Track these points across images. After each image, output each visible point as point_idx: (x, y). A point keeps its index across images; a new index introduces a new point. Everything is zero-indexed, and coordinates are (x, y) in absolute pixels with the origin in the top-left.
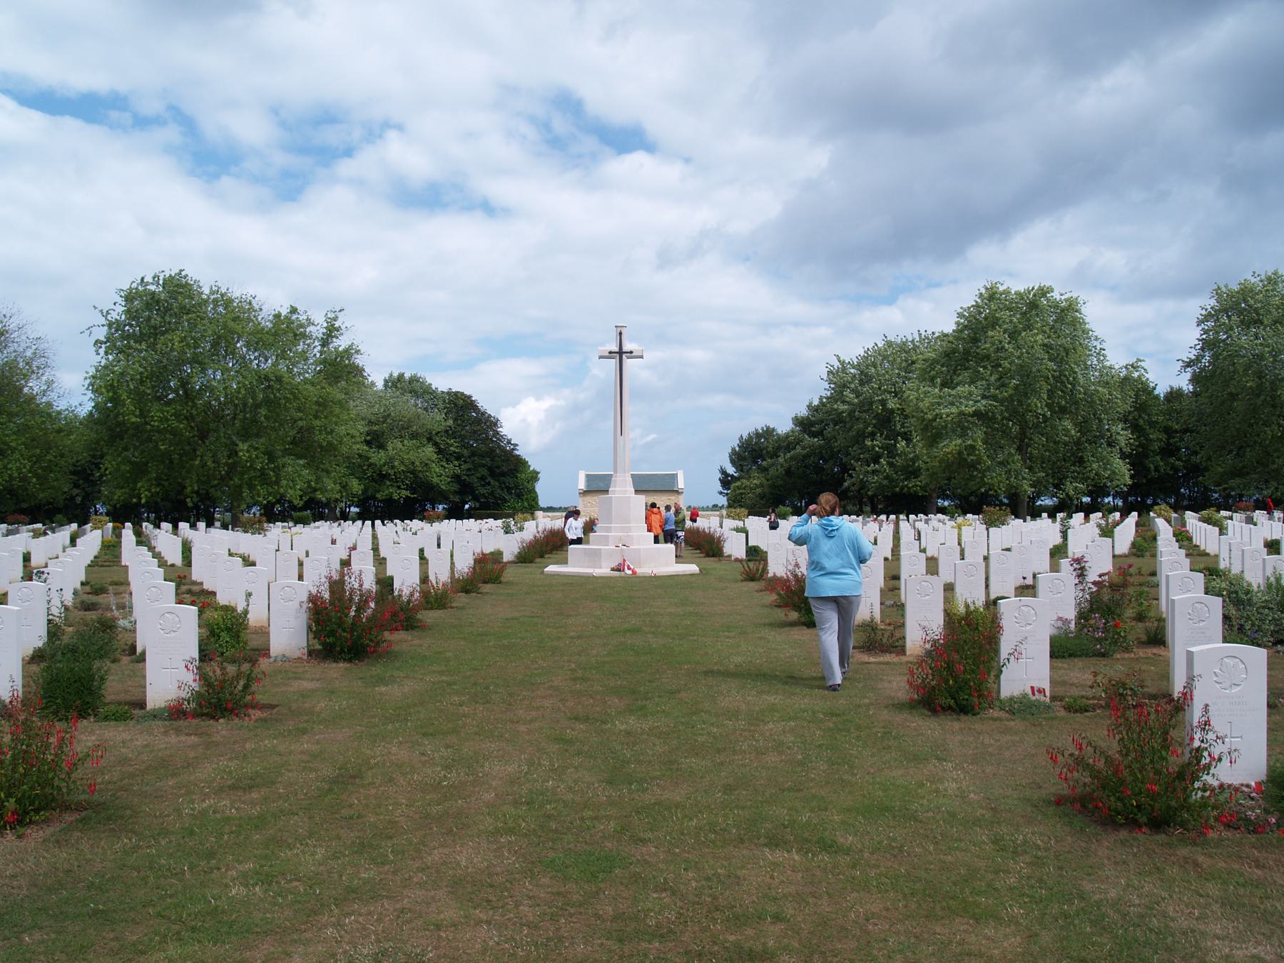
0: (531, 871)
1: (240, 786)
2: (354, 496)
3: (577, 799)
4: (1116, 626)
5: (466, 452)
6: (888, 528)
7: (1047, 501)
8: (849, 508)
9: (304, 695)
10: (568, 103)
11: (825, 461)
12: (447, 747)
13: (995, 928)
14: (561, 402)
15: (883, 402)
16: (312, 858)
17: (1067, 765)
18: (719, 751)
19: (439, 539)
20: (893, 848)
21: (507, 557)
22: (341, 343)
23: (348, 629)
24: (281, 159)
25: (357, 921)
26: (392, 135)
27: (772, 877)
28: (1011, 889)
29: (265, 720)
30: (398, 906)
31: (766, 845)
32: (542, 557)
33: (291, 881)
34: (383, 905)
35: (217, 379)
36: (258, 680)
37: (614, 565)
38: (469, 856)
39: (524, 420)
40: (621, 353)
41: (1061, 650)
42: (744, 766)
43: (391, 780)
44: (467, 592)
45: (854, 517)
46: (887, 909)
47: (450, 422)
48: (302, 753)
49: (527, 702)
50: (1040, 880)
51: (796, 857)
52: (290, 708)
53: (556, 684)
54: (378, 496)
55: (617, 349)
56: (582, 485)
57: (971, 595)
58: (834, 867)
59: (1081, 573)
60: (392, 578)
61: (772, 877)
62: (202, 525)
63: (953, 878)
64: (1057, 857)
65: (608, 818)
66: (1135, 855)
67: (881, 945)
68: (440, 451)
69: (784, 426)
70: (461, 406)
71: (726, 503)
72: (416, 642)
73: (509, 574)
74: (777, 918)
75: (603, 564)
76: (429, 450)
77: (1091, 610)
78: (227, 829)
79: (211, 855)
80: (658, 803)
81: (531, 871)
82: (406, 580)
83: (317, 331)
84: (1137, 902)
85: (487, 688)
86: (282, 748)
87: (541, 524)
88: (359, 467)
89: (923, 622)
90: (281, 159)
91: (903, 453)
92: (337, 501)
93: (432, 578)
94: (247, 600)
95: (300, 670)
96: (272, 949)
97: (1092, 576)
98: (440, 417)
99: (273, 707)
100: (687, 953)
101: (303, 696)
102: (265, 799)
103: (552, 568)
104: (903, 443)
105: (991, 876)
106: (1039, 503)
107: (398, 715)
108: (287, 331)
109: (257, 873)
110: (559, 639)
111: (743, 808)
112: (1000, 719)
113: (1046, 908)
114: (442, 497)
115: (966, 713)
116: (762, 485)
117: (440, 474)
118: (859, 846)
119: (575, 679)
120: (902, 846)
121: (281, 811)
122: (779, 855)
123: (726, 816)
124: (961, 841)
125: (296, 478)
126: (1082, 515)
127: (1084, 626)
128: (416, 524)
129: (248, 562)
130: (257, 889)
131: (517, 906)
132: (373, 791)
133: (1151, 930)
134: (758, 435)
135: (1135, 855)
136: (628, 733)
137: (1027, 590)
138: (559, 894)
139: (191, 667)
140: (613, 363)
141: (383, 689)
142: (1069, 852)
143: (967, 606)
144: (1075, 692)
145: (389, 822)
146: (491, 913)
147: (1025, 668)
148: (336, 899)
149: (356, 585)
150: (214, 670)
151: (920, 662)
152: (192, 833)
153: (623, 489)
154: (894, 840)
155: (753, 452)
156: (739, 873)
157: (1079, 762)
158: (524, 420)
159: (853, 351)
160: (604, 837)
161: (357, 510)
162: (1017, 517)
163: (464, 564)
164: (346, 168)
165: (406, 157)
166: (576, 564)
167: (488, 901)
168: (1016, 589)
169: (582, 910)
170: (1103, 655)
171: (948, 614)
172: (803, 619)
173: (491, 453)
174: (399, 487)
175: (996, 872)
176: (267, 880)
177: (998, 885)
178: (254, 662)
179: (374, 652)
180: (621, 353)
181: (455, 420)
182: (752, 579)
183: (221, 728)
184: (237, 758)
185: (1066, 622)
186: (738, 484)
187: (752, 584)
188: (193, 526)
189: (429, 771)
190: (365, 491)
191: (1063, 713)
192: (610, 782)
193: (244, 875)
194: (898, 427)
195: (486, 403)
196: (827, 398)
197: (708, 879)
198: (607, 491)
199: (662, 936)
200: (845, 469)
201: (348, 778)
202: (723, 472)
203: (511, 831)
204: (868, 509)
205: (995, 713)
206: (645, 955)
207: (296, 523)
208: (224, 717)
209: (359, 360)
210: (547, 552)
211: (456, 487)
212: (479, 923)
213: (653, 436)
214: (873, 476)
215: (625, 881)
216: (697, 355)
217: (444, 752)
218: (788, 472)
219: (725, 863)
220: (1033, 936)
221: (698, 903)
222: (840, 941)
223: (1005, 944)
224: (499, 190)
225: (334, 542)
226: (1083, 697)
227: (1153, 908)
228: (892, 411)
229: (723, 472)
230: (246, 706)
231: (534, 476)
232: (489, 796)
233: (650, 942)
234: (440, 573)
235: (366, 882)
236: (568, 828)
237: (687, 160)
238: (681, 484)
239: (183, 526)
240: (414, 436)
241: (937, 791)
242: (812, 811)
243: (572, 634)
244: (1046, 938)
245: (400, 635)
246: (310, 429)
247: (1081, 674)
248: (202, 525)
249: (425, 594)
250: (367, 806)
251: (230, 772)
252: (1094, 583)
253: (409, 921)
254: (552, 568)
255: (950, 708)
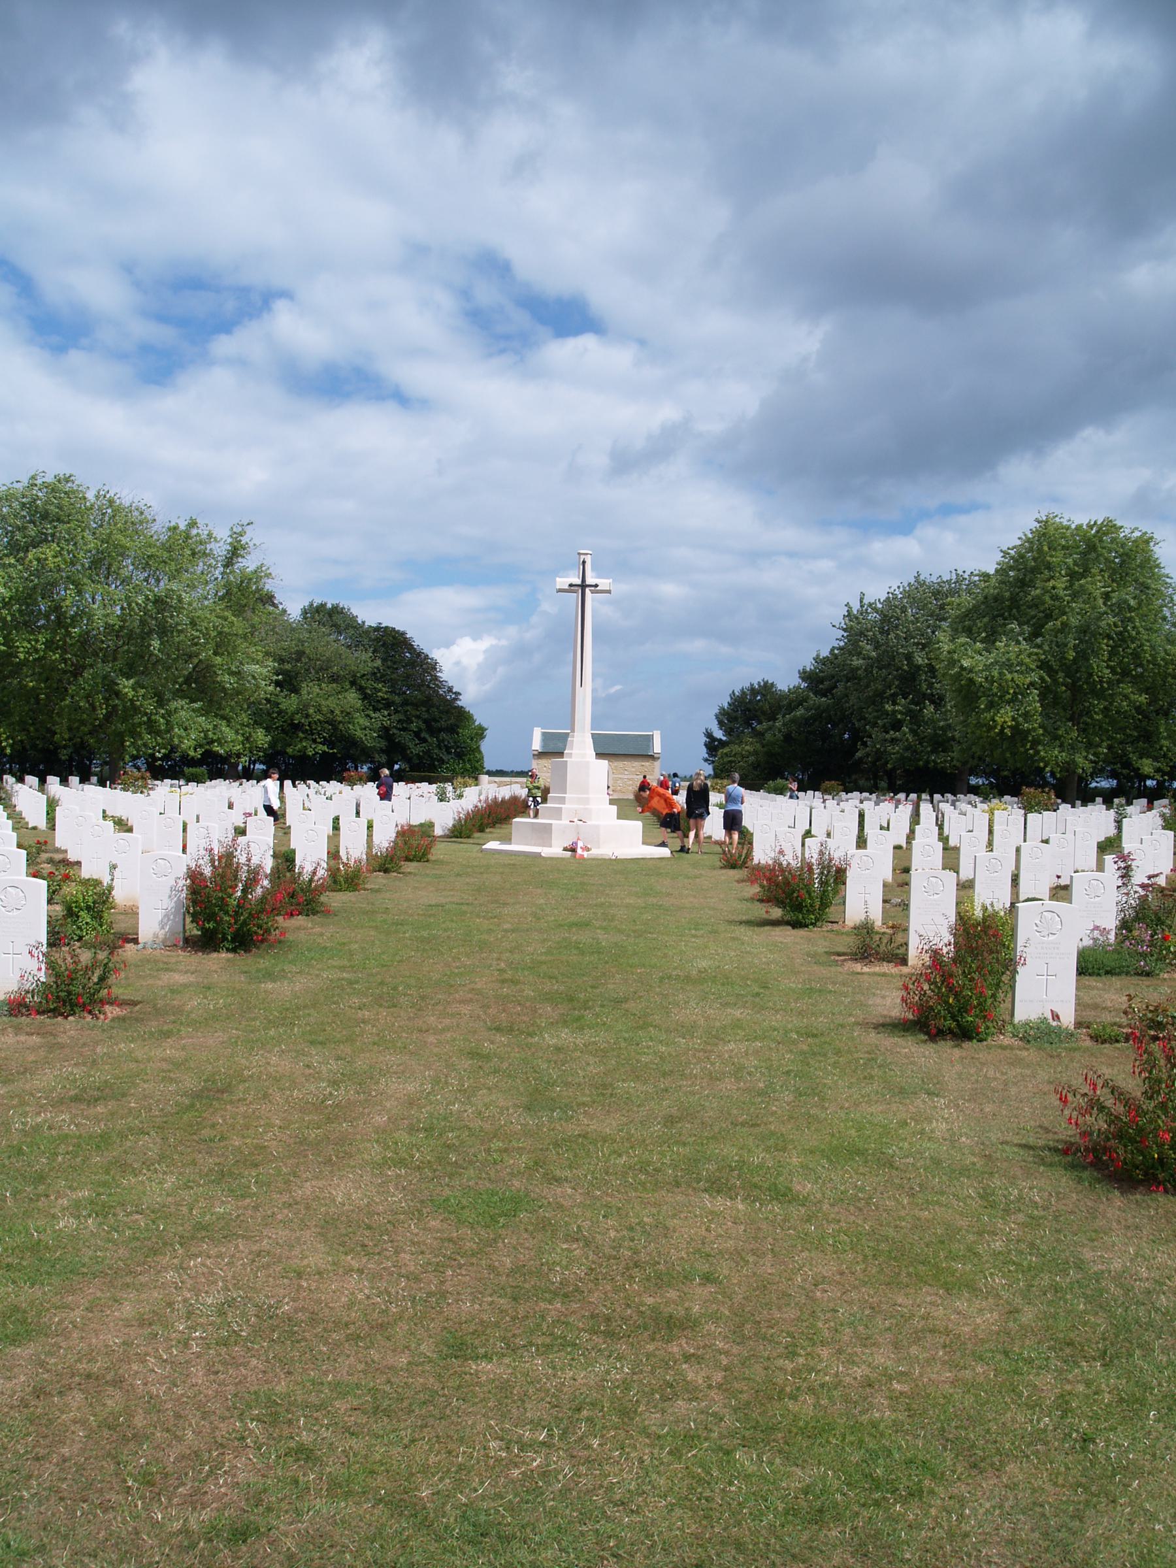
0: (419, 1211)
1: (81, 1098)
2: (259, 749)
3: (487, 1126)
4: (1165, 938)
5: (397, 699)
6: (906, 810)
7: (1106, 784)
8: (861, 782)
9: (174, 990)
10: (493, 265)
11: (834, 726)
12: (338, 1058)
13: (968, 1300)
14: (504, 642)
15: (909, 657)
16: (159, 1187)
17: (1079, 1109)
18: (664, 1074)
19: (358, 805)
20: (860, 1199)
21: (438, 831)
22: (248, 564)
23: (225, 915)
24: (144, 330)
25: (203, 1265)
26: (280, 305)
27: (708, 1230)
28: (996, 1254)
29: (123, 1019)
30: (255, 1248)
31: (706, 1190)
32: (481, 830)
33: (131, 1214)
34: (237, 1246)
35: (103, 606)
36: (116, 970)
37: (567, 844)
38: (346, 1191)
39: (458, 663)
40: (583, 586)
41: (1089, 966)
42: (693, 1093)
43: (265, 1096)
44: (386, 871)
45: (866, 794)
46: (842, 1274)
47: (378, 663)
48: (164, 1060)
49: (440, 1007)
50: (1032, 1245)
51: (740, 1207)
52: (155, 1006)
53: (478, 986)
54: (289, 750)
55: (579, 582)
56: (537, 745)
57: (991, 894)
58: (784, 1220)
59: (1126, 874)
60: (294, 851)
61: (708, 1230)
62: (74, 780)
63: (927, 1239)
64: (1056, 1218)
65: (520, 1151)
66: (1151, 1218)
67: (828, 1315)
68: (365, 697)
69: (786, 680)
70: (391, 644)
71: (712, 773)
72: (317, 930)
73: (440, 851)
74: (707, 1279)
75: (554, 842)
76: (352, 698)
77: (1137, 919)
78: (62, 1149)
79: (41, 1178)
80: (585, 1136)
81: (419, 1211)
82: (310, 857)
83: (220, 549)
84: (1145, 1275)
85: (395, 989)
86: (139, 1054)
87: (485, 791)
88: (265, 715)
89: (931, 925)
90: (144, 330)
91: (933, 721)
92: (238, 756)
93: (343, 854)
94: (112, 874)
95: (173, 960)
96: (99, 1294)
97: (1139, 878)
98: (366, 656)
99: (134, 1003)
100: (592, 1316)
101: (172, 991)
102: (112, 1114)
103: (493, 845)
104: (932, 708)
105: (971, 1238)
106: (1093, 785)
107: (285, 1018)
108: (183, 547)
109: (92, 1203)
110: (490, 931)
111: (684, 1144)
112: (1011, 1048)
113: (1034, 1278)
114: (365, 754)
115: (970, 1039)
116: (756, 753)
117: (364, 727)
118: (819, 1196)
119: (503, 981)
120: (871, 1198)
121: (130, 1129)
122: (721, 1203)
123: (662, 1154)
124: (942, 1193)
125: (190, 727)
126: (1144, 801)
127: (1127, 938)
128: (333, 787)
129: (123, 825)
130: (90, 1221)
131: (397, 1252)
132: (242, 1109)
133: (1157, 1310)
134: (753, 691)
135: (1151, 1218)
136: (558, 1049)
137: (1061, 892)
138: (450, 1240)
139: (35, 952)
140: (575, 597)
141: (270, 986)
142: (1071, 1212)
143: (985, 909)
144: (1107, 1018)
145: (257, 1147)
146: (364, 1260)
147: (1045, 988)
148: (182, 1237)
149: (243, 860)
150: (63, 955)
151: (917, 978)
152: (20, 1152)
153: (581, 748)
154: (862, 1189)
155: (748, 711)
156: (671, 1223)
157: (1095, 1105)
158: (458, 663)
159: (878, 591)
160: (512, 1174)
161: (262, 767)
162: (1064, 801)
163: (384, 838)
164: (224, 345)
165: (296, 330)
166: (520, 840)
167: (364, 1246)
168: (1052, 889)
169: (474, 1260)
170: (1148, 974)
171: (963, 919)
172: (787, 918)
173: (427, 702)
174: (314, 741)
175: (980, 1234)
176: (102, 1211)
177: (980, 1249)
178: (113, 948)
179: (262, 941)
180: (583, 586)
181: (384, 660)
182: (733, 866)
183: (70, 1027)
184: (84, 1064)
185: (1104, 932)
186: (726, 750)
187: (732, 872)
188: (64, 782)
189: (312, 1088)
190: (272, 744)
191: (1088, 1043)
192: (528, 1108)
193: (77, 1204)
194: (924, 686)
195: (420, 641)
196: (840, 648)
197: (631, 1229)
198: (561, 754)
199: (566, 1296)
200: (858, 736)
201: (214, 1092)
202: (709, 735)
203: (401, 1163)
204: (883, 784)
205: (1005, 1040)
206: (543, 1317)
207: (188, 781)
208: (74, 1014)
209: (269, 586)
210: (488, 825)
211: (383, 744)
212: (349, 1271)
213: (618, 687)
214: (895, 745)
215: (531, 1228)
216: (670, 590)
217: (333, 1065)
218: (788, 738)
219: (654, 1211)
220: (1013, 1312)
221: (615, 1258)
222: (779, 1309)
223: (978, 1321)
224: (416, 376)
225: (231, 806)
226: (1115, 1024)
227: (1162, 1284)
228: (919, 667)
229: (709, 735)
230: (103, 1002)
231: (480, 733)
232: (381, 1120)
233: (550, 1303)
234: (353, 848)
235: (221, 1217)
236: (471, 1162)
237: (642, 342)
238: (657, 748)
239: (53, 781)
240: (334, 679)
241: (922, 1132)
242: (767, 1150)
243: (507, 926)
244: (1028, 1315)
245: (300, 920)
246: (209, 667)
247: (1114, 995)
248: (74, 780)
249: (333, 872)
250: (233, 1127)
251: (75, 1080)
252: (1143, 886)
253: (267, 1266)
254: (493, 845)
255: (951, 1031)
